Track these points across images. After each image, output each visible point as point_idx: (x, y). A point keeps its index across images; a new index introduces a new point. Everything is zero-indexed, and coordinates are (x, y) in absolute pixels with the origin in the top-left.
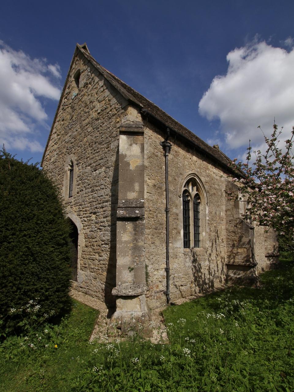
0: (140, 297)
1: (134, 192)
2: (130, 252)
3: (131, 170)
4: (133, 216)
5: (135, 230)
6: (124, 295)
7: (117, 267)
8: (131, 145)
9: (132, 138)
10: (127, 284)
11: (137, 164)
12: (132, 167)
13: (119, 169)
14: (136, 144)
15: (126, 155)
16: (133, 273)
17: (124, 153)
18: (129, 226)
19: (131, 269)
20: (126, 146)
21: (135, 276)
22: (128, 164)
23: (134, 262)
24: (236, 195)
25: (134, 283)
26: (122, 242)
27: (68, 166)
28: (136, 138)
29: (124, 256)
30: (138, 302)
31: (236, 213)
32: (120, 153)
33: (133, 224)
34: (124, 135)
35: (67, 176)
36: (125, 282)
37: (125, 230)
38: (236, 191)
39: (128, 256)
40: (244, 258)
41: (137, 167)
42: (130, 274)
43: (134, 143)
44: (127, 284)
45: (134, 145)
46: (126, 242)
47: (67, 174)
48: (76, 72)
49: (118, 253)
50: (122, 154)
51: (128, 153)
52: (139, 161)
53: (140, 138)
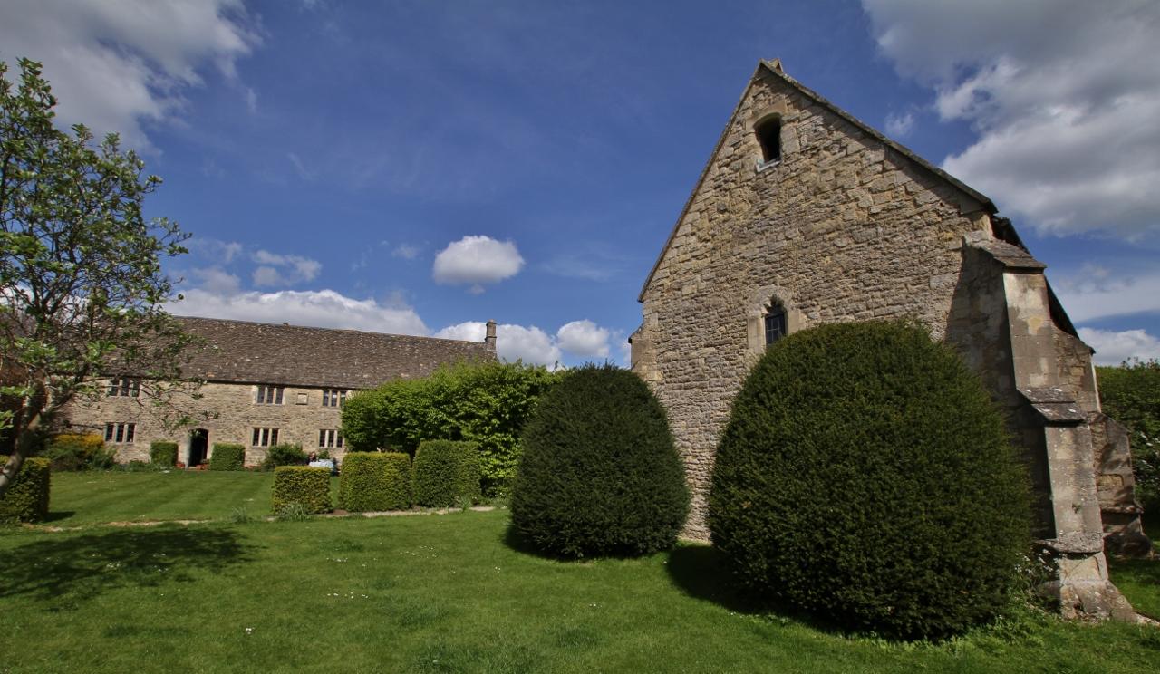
0: (1096, 555)
1: (1040, 373)
2: (1072, 479)
3: (1030, 336)
4: (1065, 418)
5: (1075, 442)
6: (1077, 551)
7: (1055, 504)
8: (1025, 291)
9: (1024, 277)
10: (1074, 533)
11: (1039, 326)
12: (1032, 331)
13: (1012, 333)
14: (1034, 289)
15: (1018, 310)
16: (1080, 515)
17: (1015, 305)
18: (1065, 434)
19: (1077, 508)
20: (1017, 293)
21: (1085, 520)
22: (1025, 325)
23: (1080, 496)
24: (1084, 362)
25: (1084, 531)
26: (1056, 461)
27: (760, 309)
28: (1034, 278)
29: (1064, 485)
30: (1095, 564)
31: (1087, 400)
32: (1009, 306)
33: (1071, 431)
34: (1011, 272)
35: (758, 328)
36: (1070, 530)
37: (1060, 442)
38: (1084, 355)
39: (1069, 485)
40: (1120, 493)
41: (1040, 329)
42: (1076, 517)
43: (1030, 287)
44: (1074, 533)
45: (1030, 291)
46: (1064, 462)
47: (758, 324)
48: (765, 117)
49: (1053, 481)
50: (1013, 308)
51: (1022, 306)
52: (1041, 319)
53: (1038, 277)
